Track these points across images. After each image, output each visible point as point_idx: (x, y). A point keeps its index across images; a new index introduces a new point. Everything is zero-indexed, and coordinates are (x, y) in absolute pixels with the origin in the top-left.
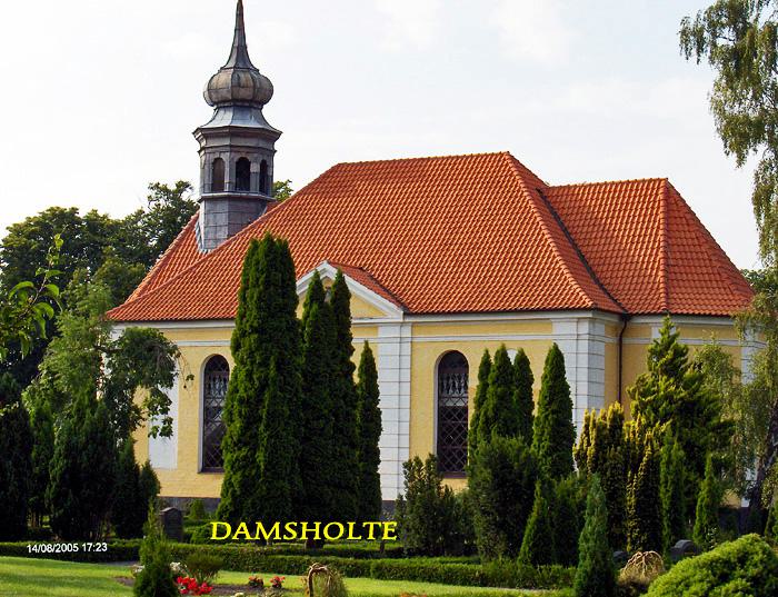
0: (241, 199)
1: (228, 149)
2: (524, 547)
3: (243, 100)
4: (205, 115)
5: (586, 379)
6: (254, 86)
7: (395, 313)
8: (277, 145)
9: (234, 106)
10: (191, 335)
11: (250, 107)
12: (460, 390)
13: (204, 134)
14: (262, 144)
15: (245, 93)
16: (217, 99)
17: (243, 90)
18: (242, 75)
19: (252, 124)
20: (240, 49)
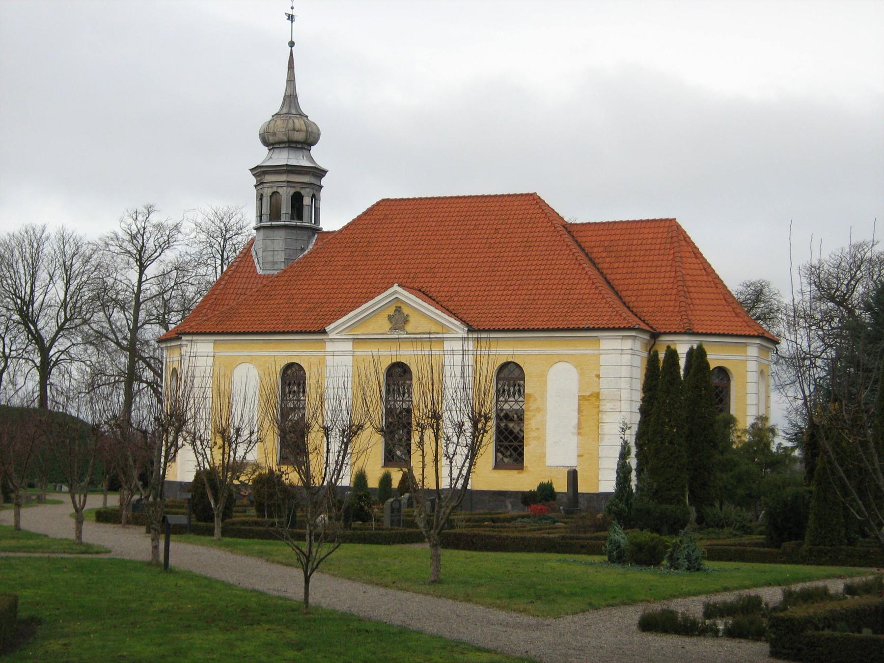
0: (296, 227)
1: (285, 184)
2: (266, 514)
3: (297, 142)
4: (261, 155)
5: (628, 387)
6: (307, 131)
7: (460, 330)
8: (324, 181)
9: (289, 147)
10: (272, 345)
11: (302, 148)
12: (404, 394)
13: (260, 172)
14: (313, 180)
15: (299, 136)
16: (270, 141)
17: (291, 133)
18: (296, 121)
19: (305, 163)
20: (291, 99)
